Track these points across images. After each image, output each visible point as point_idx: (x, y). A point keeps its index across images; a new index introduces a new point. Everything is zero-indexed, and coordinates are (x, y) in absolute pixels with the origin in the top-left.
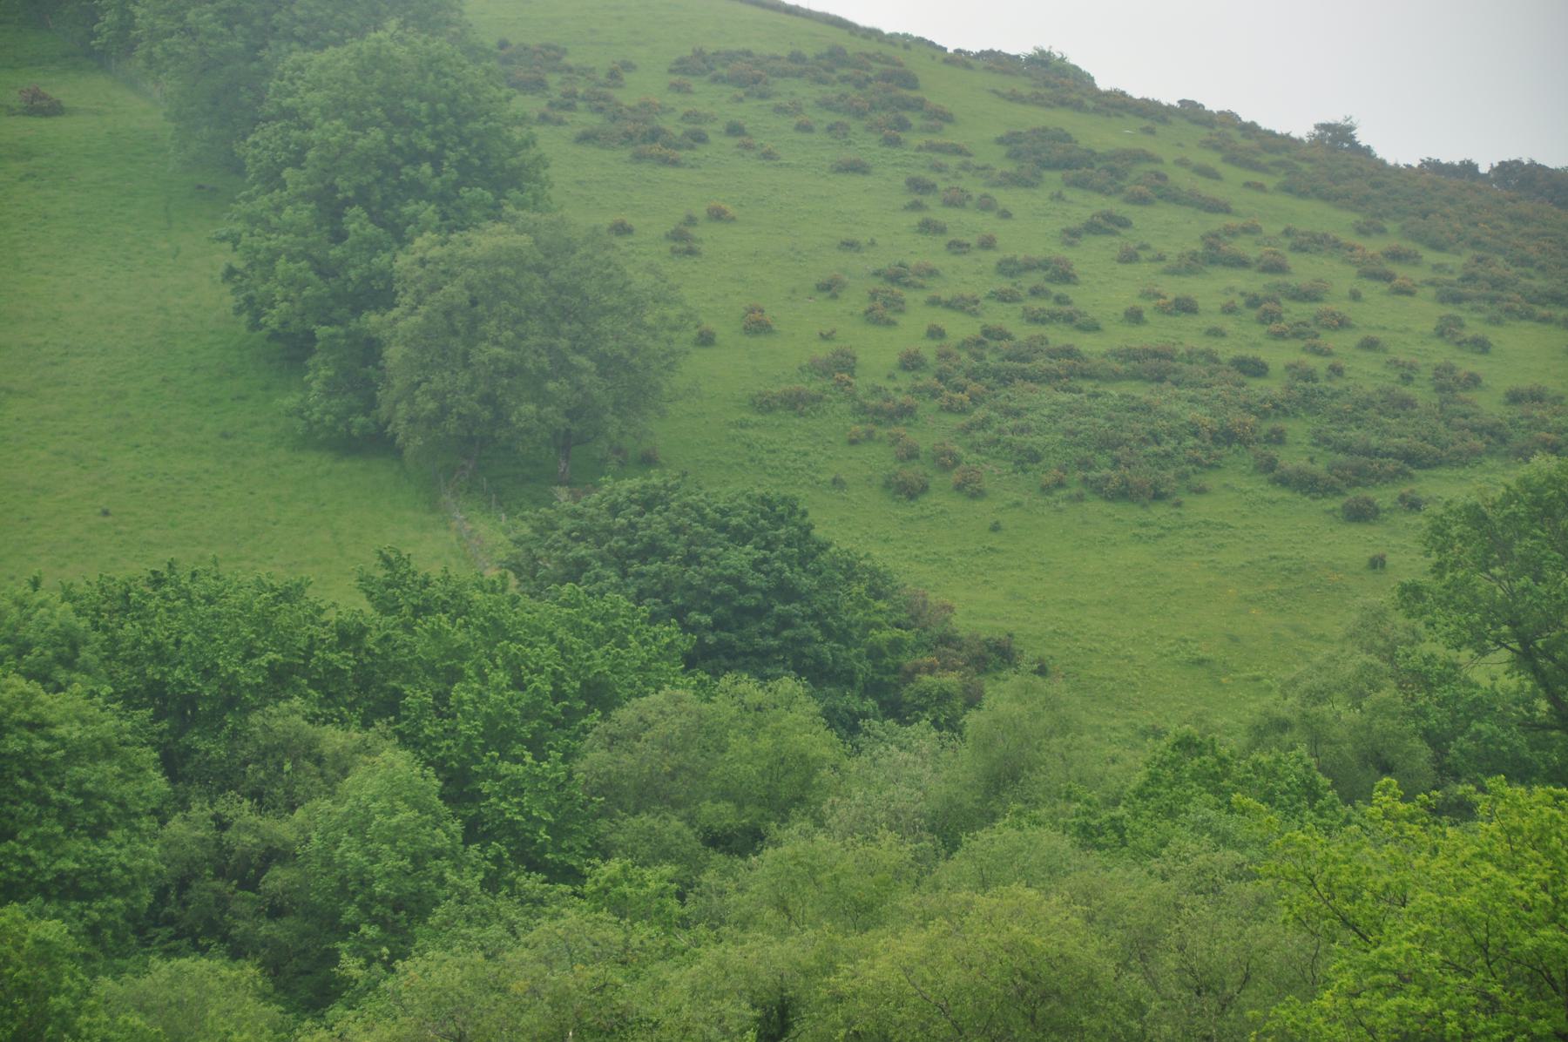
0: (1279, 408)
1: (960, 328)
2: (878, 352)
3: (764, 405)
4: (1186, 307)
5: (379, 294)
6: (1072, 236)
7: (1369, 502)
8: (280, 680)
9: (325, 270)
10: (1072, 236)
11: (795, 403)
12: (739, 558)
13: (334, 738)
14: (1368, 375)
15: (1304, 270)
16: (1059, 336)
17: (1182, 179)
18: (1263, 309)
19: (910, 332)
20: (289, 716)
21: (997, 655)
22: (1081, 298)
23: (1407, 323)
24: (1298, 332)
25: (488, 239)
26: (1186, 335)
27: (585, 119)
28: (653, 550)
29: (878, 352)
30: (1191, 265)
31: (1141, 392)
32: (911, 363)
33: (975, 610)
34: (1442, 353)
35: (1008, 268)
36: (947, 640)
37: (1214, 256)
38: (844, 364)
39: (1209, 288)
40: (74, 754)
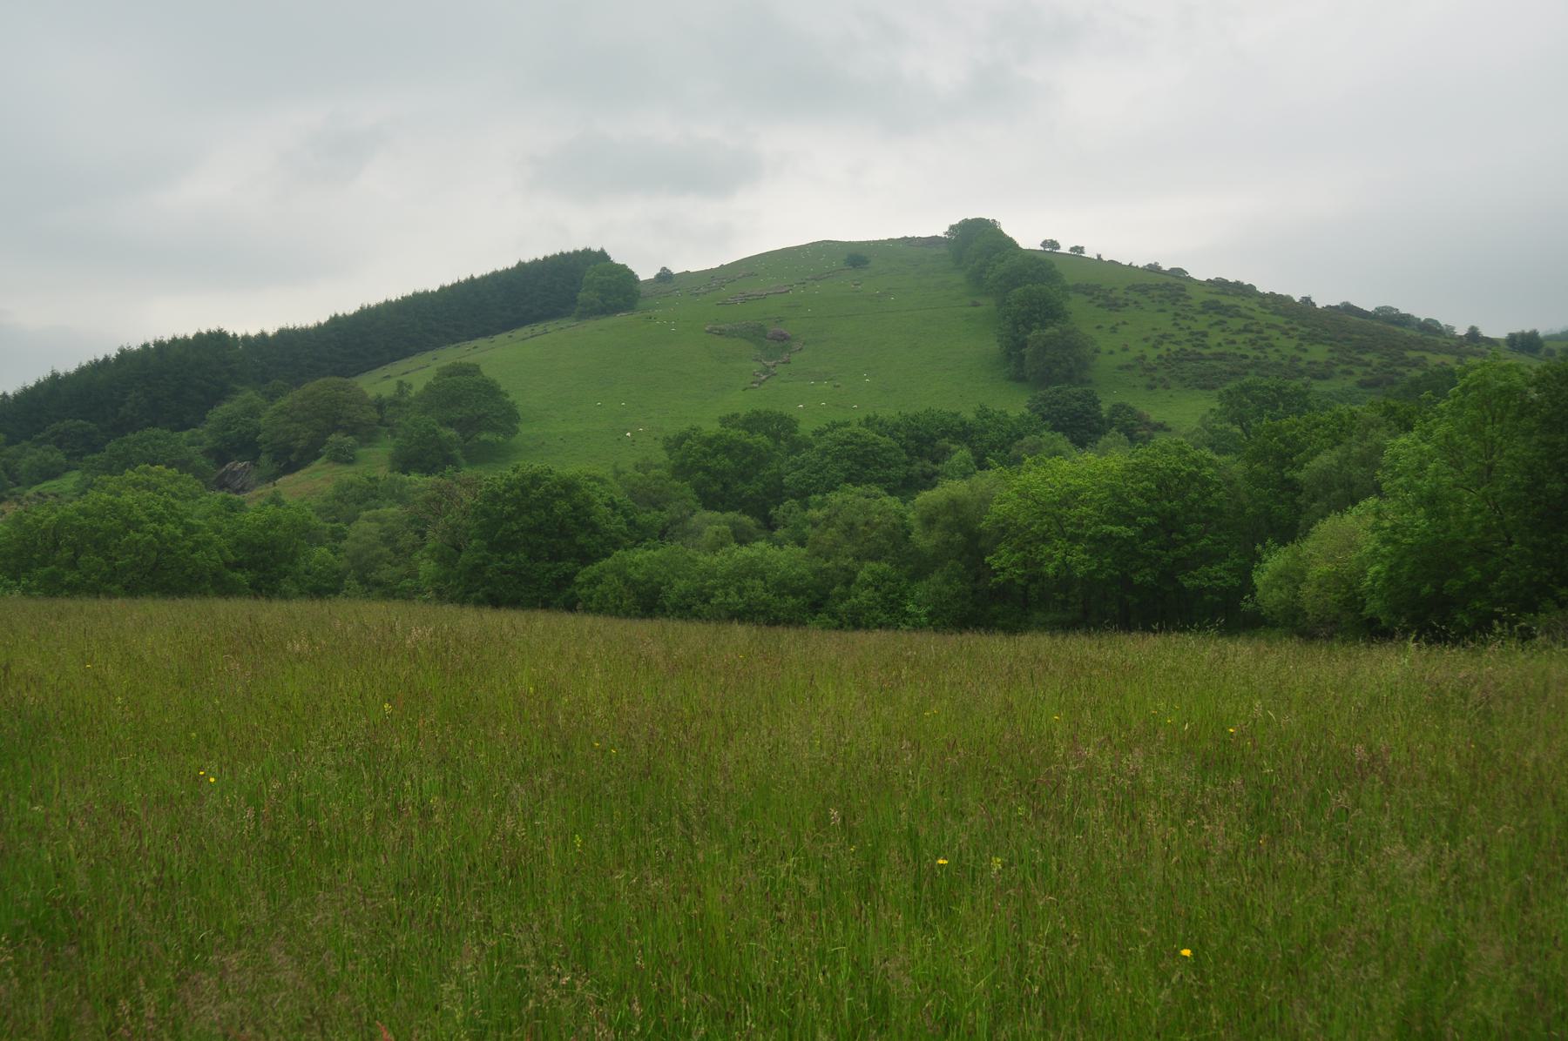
0: (1249, 366)
1: (1174, 348)
2: (1152, 354)
3: (1120, 368)
4: (1233, 342)
5: (1024, 345)
6: (1211, 326)
7: (471, 370)
8: (944, 434)
9: (1015, 339)
10: (1211, 326)
11: (1128, 367)
12: (1076, 404)
13: (953, 447)
14: (1274, 357)
15: (1267, 333)
16: (1198, 350)
17: (1244, 311)
18: (1252, 343)
19: (1162, 350)
20: (944, 442)
21: (1161, 427)
22: (1207, 341)
23: (1288, 346)
24: (1261, 348)
25: (1049, 331)
26: (1232, 349)
27: (1101, 301)
28: (1057, 403)
29: (1152, 354)
30: (1239, 332)
31: (1214, 363)
32: (1160, 357)
33: (1155, 416)
34: (1295, 352)
35: (1192, 334)
36: (1148, 423)
37: (1246, 330)
38: (1144, 357)
39: (1240, 338)
40: (884, 450)
